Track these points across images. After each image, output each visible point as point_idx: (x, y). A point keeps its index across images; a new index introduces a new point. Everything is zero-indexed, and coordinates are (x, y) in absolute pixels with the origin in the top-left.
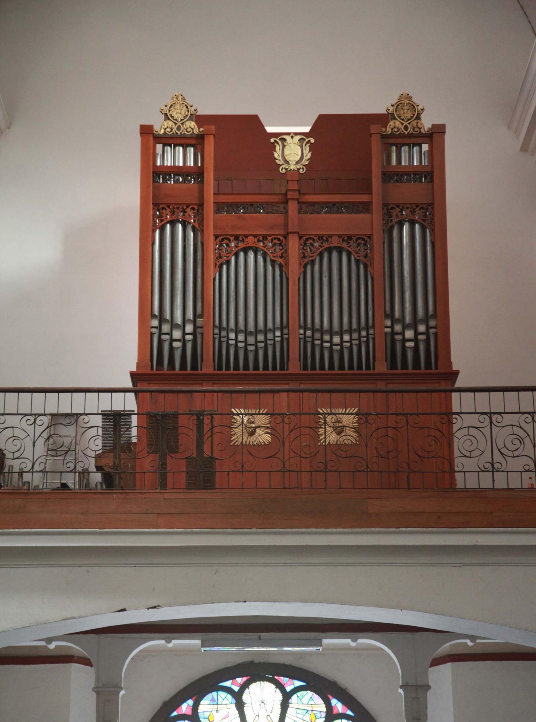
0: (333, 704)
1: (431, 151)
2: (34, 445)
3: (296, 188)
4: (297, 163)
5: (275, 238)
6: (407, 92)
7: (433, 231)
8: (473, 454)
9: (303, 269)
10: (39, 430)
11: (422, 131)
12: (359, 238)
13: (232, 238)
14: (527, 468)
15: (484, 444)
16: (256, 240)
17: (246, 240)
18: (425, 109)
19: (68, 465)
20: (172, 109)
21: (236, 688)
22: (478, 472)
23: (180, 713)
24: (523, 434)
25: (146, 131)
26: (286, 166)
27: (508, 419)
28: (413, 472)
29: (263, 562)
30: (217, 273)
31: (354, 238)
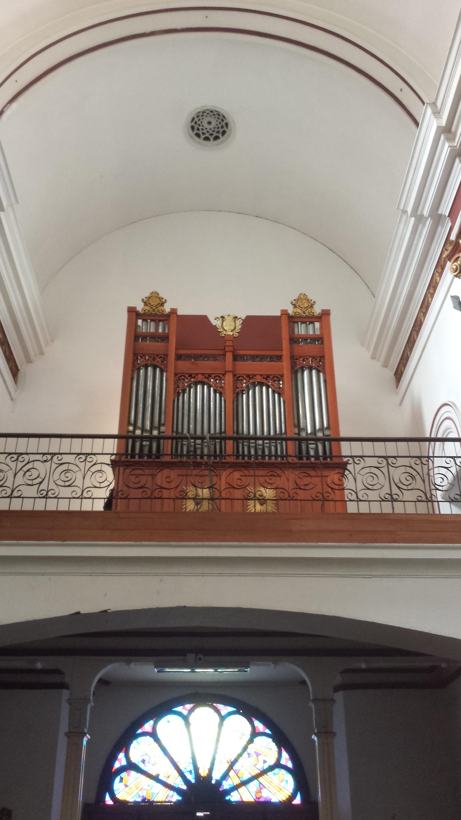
0: (256, 725)
1: (321, 327)
2: (15, 477)
3: (231, 345)
4: (232, 331)
5: (217, 376)
6: (304, 293)
7: (324, 373)
8: (375, 487)
9: (236, 395)
10: (20, 465)
11: (315, 314)
12: (275, 377)
13: (187, 376)
14: (420, 498)
15: (383, 480)
16: (204, 377)
17: (196, 377)
18: (316, 302)
19: (41, 493)
20: (150, 299)
21: (185, 713)
22: (380, 501)
23: (144, 731)
24: (414, 473)
25: (132, 311)
26: (224, 332)
27: (401, 461)
28: (327, 500)
29: (201, 572)
30: (176, 398)
31: (271, 377)
